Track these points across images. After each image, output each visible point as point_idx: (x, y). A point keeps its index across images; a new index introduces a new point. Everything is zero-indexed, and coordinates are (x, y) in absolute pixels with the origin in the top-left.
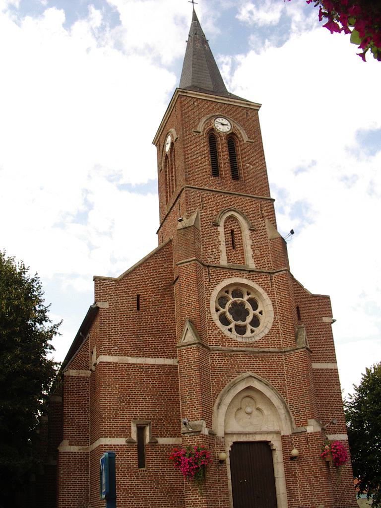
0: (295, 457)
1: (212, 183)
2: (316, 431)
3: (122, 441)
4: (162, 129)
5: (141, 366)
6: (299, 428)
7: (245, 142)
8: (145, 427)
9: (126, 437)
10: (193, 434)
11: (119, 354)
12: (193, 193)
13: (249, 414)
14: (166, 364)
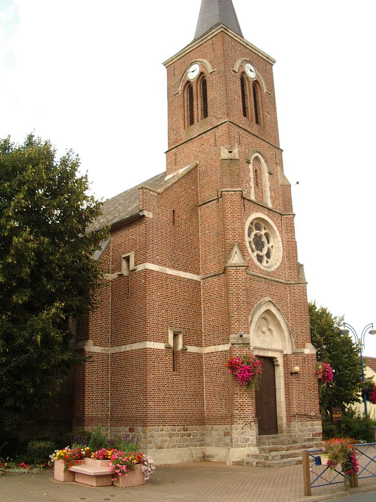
0: (296, 373)
1: (243, 122)
2: (312, 353)
3: (161, 346)
4: (184, 54)
5: (176, 278)
6: (298, 349)
7: (265, 92)
8: (178, 335)
9: (165, 343)
10: (241, 345)
11: (159, 264)
12: (233, 127)
13: (264, 333)
14: (193, 279)
